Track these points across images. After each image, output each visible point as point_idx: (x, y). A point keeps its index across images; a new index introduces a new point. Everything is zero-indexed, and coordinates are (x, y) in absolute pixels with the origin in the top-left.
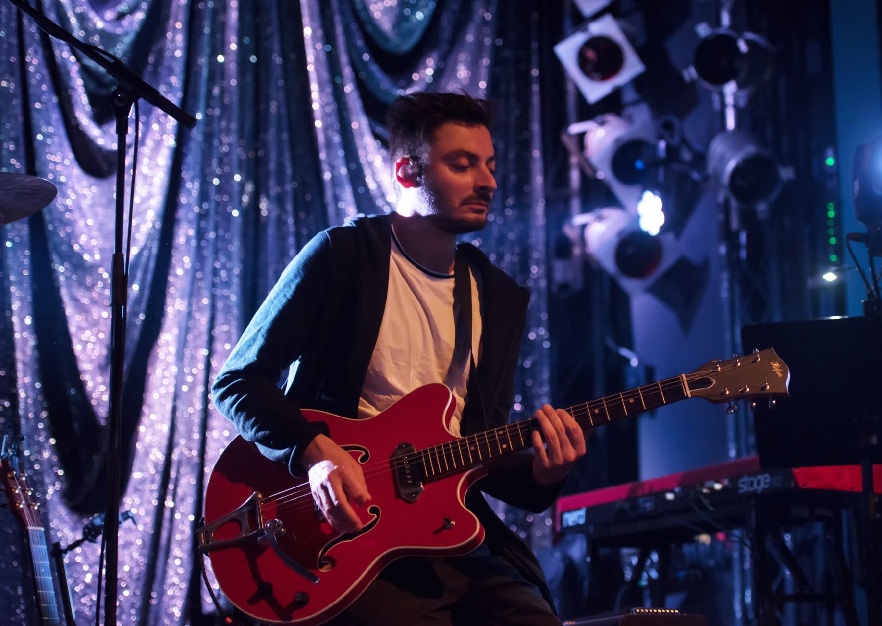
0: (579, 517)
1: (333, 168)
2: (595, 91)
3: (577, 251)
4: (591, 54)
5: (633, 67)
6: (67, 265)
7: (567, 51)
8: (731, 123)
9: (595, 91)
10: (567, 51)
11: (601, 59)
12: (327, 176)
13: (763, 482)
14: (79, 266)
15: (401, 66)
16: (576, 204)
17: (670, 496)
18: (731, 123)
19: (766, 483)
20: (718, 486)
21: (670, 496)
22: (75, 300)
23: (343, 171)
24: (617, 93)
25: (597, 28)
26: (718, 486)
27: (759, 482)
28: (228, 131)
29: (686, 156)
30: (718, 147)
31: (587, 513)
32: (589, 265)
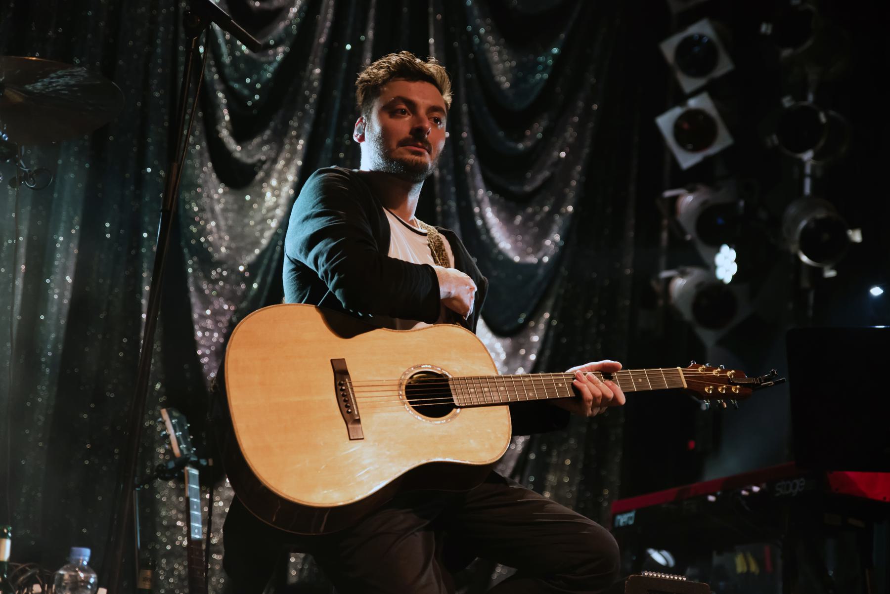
0: (630, 518)
1: (444, 203)
2: (687, 160)
3: (661, 302)
4: (686, 126)
5: (723, 140)
6: (195, 259)
7: (665, 122)
8: (807, 190)
9: (687, 160)
10: (665, 122)
11: (694, 131)
12: (439, 209)
13: (799, 485)
14: (207, 261)
15: (516, 124)
16: (663, 261)
17: (712, 498)
18: (807, 190)
19: (800, 487)
20: (756, 489)
21: (712, 498)
22: (200, 290)
23: (453, 204)
24: (707, 161)
25: (693, 103)
26: (756, 489)
27: (794, 486)
28: (560, 467)
29: (763, 215)
30: (792, 210)
31: (636, 515)
32: (670, 312)
